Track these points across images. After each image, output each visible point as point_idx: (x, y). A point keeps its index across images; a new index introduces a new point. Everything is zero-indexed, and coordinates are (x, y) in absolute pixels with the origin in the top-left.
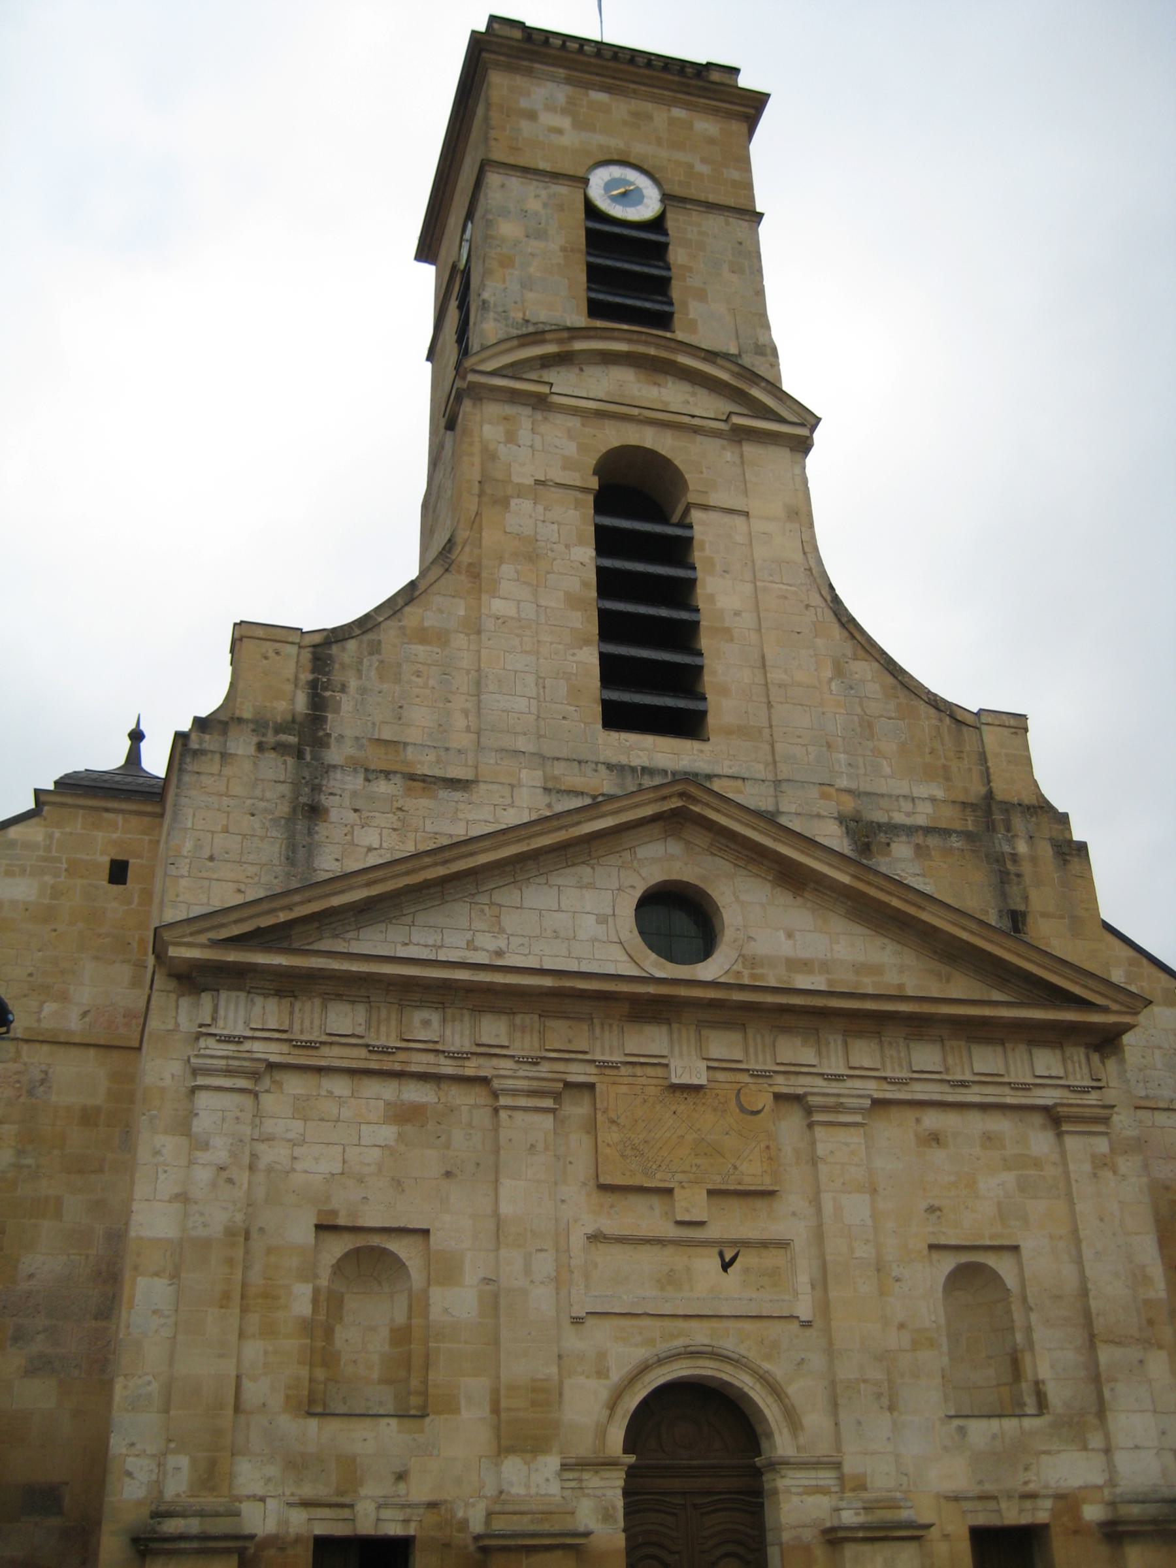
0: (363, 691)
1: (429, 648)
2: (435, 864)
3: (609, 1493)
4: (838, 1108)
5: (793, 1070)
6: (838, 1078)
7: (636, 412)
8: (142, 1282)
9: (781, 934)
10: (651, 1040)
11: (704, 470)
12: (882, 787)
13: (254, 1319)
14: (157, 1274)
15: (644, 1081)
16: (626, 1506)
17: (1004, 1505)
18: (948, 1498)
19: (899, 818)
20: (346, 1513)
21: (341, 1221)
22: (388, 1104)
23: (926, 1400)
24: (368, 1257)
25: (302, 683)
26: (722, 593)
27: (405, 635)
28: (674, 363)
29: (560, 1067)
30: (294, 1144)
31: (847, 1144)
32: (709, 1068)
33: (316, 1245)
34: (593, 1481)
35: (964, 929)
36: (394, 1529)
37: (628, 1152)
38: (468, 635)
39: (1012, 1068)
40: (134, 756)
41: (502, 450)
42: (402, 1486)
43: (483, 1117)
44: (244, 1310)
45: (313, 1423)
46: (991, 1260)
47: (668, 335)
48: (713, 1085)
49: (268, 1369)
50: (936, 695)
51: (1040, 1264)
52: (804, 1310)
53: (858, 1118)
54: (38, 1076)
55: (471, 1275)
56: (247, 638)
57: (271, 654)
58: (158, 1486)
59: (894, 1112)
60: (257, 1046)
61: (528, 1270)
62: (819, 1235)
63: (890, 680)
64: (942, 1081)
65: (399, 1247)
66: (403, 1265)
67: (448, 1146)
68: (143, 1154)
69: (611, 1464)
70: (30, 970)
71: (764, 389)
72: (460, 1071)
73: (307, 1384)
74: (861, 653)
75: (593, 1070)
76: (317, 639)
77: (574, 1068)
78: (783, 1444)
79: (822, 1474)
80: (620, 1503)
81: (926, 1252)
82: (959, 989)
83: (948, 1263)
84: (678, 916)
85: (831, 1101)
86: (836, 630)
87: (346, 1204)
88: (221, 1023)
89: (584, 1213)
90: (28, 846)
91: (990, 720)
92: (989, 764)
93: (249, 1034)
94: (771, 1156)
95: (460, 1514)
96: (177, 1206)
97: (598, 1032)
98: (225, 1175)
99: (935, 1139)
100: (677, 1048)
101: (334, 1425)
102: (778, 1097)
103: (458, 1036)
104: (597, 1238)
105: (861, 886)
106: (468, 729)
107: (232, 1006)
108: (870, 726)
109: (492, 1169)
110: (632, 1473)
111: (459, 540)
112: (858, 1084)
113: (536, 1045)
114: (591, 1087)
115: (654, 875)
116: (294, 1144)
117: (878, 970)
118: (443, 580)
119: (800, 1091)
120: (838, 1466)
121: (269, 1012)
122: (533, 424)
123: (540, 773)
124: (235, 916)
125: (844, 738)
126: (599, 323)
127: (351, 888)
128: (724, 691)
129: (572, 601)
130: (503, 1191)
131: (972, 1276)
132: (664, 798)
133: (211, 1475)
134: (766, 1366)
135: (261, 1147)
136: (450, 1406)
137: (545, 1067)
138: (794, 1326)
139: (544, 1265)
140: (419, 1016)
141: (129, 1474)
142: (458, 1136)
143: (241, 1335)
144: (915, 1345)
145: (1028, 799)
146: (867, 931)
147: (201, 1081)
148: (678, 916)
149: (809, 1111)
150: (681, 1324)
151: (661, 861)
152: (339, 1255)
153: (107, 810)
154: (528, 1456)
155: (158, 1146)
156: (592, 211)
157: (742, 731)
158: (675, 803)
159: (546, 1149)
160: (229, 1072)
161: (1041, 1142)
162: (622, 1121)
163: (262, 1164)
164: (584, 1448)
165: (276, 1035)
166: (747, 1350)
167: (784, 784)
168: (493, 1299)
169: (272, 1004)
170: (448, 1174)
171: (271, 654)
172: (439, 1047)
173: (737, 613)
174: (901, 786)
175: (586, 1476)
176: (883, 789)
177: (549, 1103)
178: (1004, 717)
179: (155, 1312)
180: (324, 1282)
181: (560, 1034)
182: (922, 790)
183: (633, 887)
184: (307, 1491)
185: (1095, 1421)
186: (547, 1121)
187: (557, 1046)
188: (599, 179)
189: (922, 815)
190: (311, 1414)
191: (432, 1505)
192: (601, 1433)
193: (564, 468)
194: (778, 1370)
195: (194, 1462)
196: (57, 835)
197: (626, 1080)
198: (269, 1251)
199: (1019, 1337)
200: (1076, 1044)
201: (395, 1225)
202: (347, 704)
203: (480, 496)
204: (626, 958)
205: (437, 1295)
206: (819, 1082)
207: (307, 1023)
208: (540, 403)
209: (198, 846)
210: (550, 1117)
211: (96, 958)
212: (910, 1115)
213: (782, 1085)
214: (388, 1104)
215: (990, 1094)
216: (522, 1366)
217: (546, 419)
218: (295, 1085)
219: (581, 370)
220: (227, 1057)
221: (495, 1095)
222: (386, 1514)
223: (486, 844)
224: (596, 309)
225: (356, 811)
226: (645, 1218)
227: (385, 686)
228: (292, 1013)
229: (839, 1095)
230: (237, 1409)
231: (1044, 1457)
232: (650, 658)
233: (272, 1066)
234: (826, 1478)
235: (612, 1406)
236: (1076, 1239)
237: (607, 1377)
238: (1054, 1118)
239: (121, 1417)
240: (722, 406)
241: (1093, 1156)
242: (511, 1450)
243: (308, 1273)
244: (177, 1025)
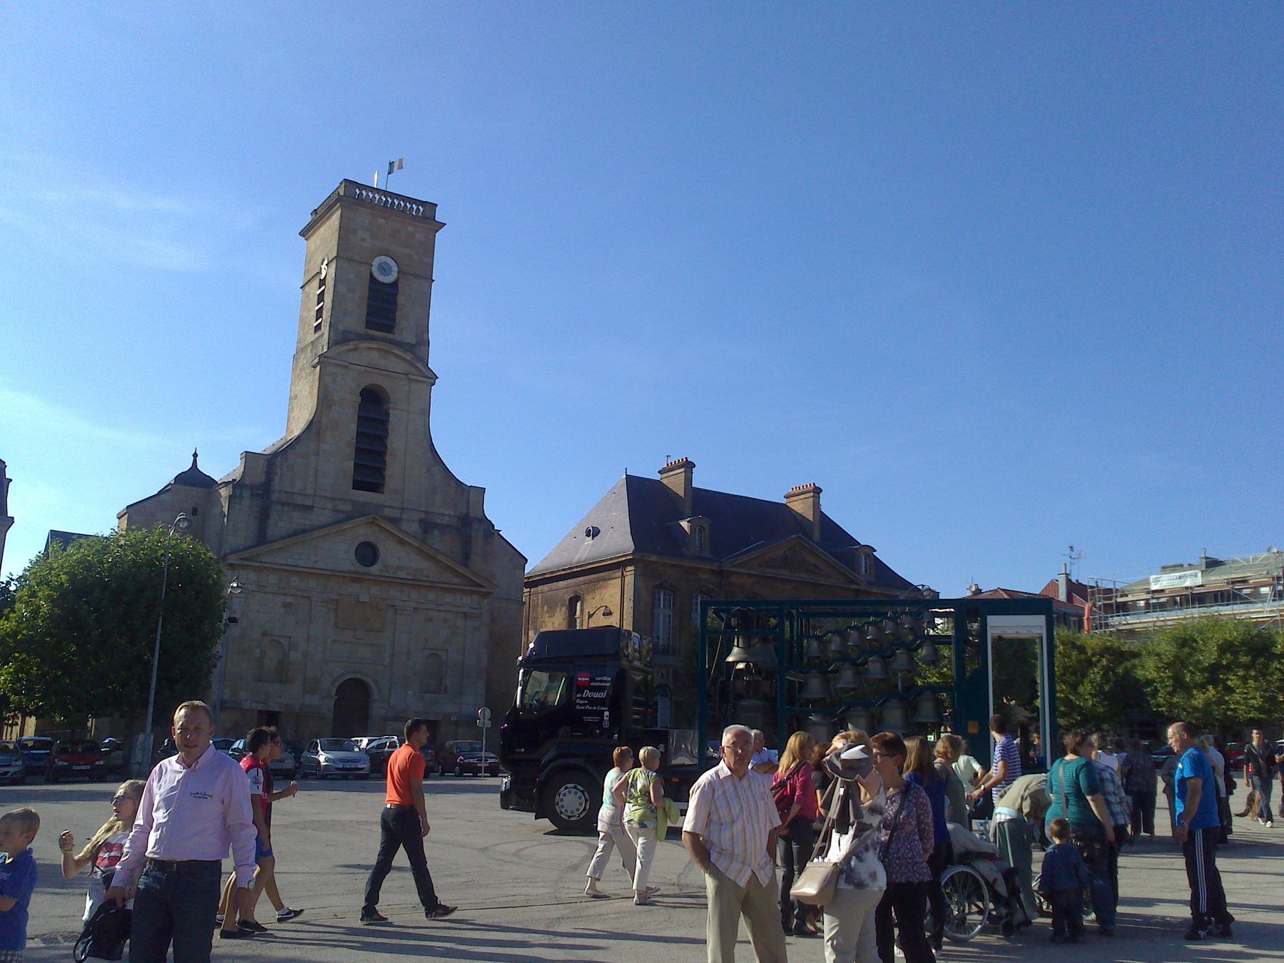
19: (438, 521)
26: (397, 442)
47: (390, 336)
56: (249, 457)
78: (376, 696)
84: (367, 553)
86: (430, 456)
99: (430, 619)
126: (369, 331)
145: (480, 516)
148: (367, 553)
151: (362, 532)
156: (371, 275)
188: (376, 262)
189: (446, 521)
198: (1179, 684)
202: (277, 479)
224: (369, 325)
232: (370, 465)
235: (333, 683)
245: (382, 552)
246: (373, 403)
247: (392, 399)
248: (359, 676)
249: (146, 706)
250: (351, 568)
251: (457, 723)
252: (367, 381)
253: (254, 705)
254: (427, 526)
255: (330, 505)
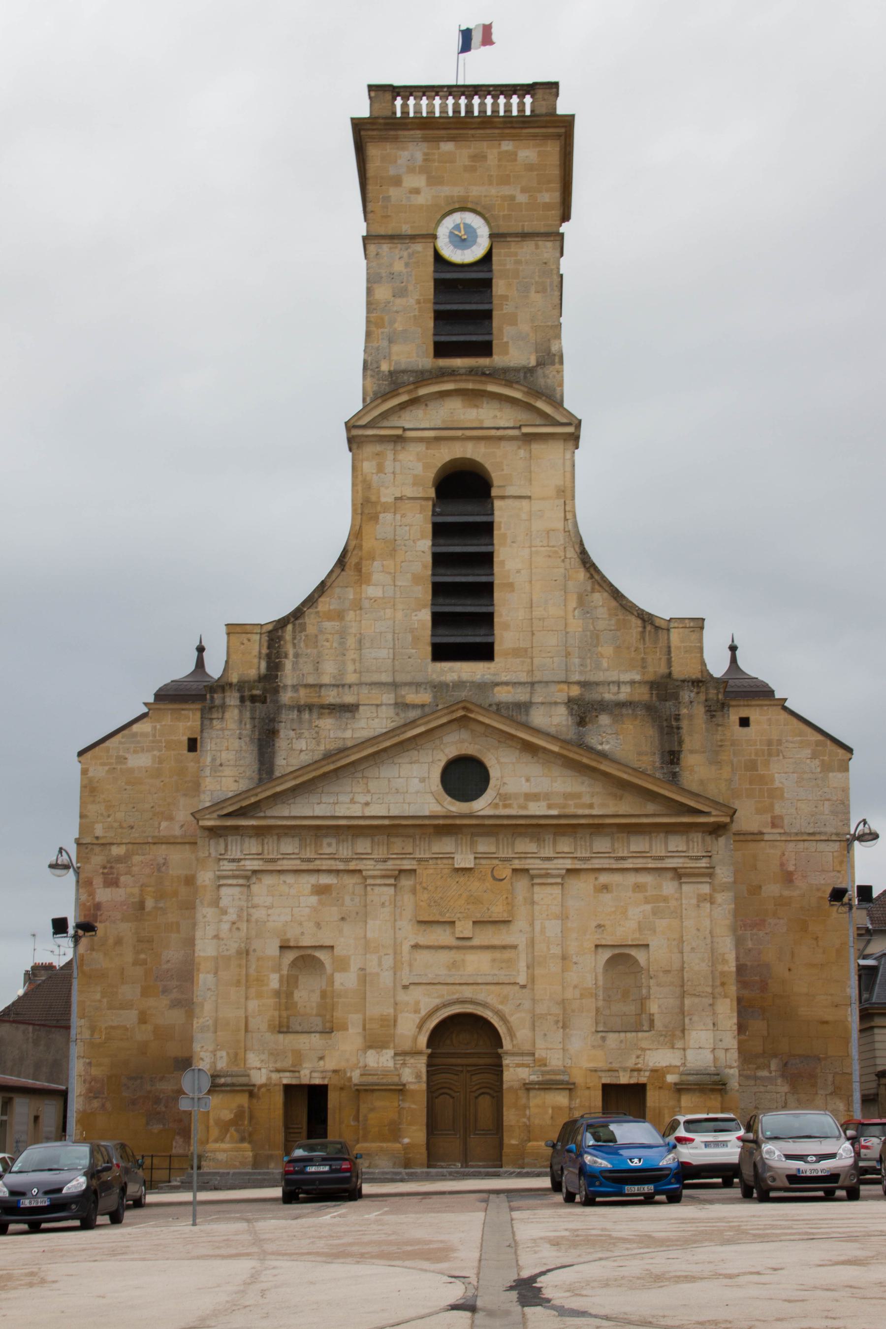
0: (297, 656)
1: (333, 623)
2: (328, 764)
3: (419, 1065)
4: (547, 875)
5: (523, 856)
6: (549, 859)
7: (459, 433)
8: (201, 976)
9: (523, 780)
10: (446, 845)
11: (505, 467)
12: (600, 676)
13: (252, 991)
14: (208, 972)
15: (442, 866)
16: (428, 1071)
17: (621, 1074)
18: (591, 1071)
19: (608, 696)
20: (297, 1074)
21: (292, 944)
22: (313, 885)
23: (584, 1023)
24: (305, 960)
25: (263, 656)
27: (319, 617)
28: (485, 391)
29: (398, 862)
30: (268, 908)
31: (551, 894)
32: (475, 858)
33: (280, 956)
34: (411, 1061)
35: (626, 773)
36: (317, 1081)
37: (432, 904)
38: (355, 611)
39: (654, 848)
40: (200, 663)
41: (375, 478)
42: (321, 1063)
43: (359, 889)
44: (247, 988)
45: (281, 1036)
46: (633, 952)
47: (482, 362)
48: (478, 867)
49: (260, 1010)
50: (643, 611)
51: (659, 953)
52: (522, 980)
53: (559, 880)
54: (162, 861)
55: (354, 967)
57: (245, 641)
58: (214, 1063)
59: (583, 876)
60: (248, 863)
61: (380, 964)
62: (532, 943)
63: (614, 603)
64: (609, 857)
65: (321, 955)
66: (323, 964)
67: (343, 905)
68: (199, 916)
69: (420, 1053)
70: (152, 805)
71: (545, 401)
72: (347, 868)
73: (278, 1019)
74: (597, 587)
75: (415, 862)
76: (270, 627)
77: (405, 862)
78: (507, 1044)
79: (526, 1058)
80: (424, 1070)
81: (593, 949)
82: (625, 807)
83: (607, 954)
84: (465, 776)
85: (543, 872)
87: (292, 935)
88: (229, 853)
89: (410, 934)
90: (144, 735)
91: (676, 625)
92: (672, 655)
93: (243, 857)
94: (510, 904)
95: (348, 1075)
96: (215, 941)
97: (418, 843)
98: (235, 926)
99: (605, 888)
100: (460, 849)
101: (290, 1037)
102: (515, 871)
103: (345, 851)
104: (416, 947)
105: (565, 752)
106: (355, 671)
107: (234, 844)
108: (598, 637)
109: (363, 914)
110: (430, 1057)
111: (350, 548)
112: (561, 861)
113: (385, 852)
114: (415, 871)
115: (452, 752)
116: (268, 908)
117: (578, 796)
118: (341, 577)
119: (527, 867)
120: (533, 1054)
121: (252, 846)
122: (394, 454)
123: (392, 696)
124: (230, 802)
125: (579, 648)
126: (444, 362)
127: (286, 781)
128: (506, 627)
129: (416, 579)
130: (368, 926)
131: (621, 960)
132: (453, 712)
133: (235, 1058)
134: (500, 1007)
135: (252, 911)
136: (344, 1028)
137: (390, 863)
138: (517, 988)
139: (388, 961)
140: (325, 841)
141: (202, 1059)
142: (347, 899)
143: (247, 998)
144: (582, 996)
146: (576, 774)
147: (222, 882)
148: (465, 776)
149: (532, 877)
150: (457, 987)
152: (292, 959)
153: (183, 709)
154: (379, 1050)
155: (205, 912)
157: (517, 652)
158: (461, 713)
159: (390, 904)
160: (235, 877)
161: (669, 887)
162: (429, 888)
163: (253, 919)
164: (407, 1046)
165: (256, 857)
166: (491, 1000)
167: (536, 685)
168: (364, 977)
169: (253, 841)
170: (343, 919)
171: (245, 641)
172: (336, 856)
173: (518, 571)
174: (613, 676)
175: (407, 1058)
176: (602, 679)
177: (392, 881)
178: (687, 621)
179: (209, 989)
180: (285, 972)
181: (398, 845)
182: (626, 677)
183: (440, 760)
184: (279, 1065)
185: (680, 1034)
186: (391, 890)
187: (396, 851)
188: (444, 231)
189: (624, 694)
190: (280, 1032)
191: (335, 1071)
192: (415, 1039)
193: (414, 484)
194: (506, 1009)
195: (228, 1054)
196: (158, 727)
197: (432, 867)
198: (258, 959)
199: (644, 991)
200: (697, 832)
201: (317, 944)
202: (288, 664)
203: (361, 514)
204: (434, 801)
205: (339, 978)
206: (538, 861)
207: (271, 848)
208: (398, 440)
209: (214, 760)
210: (393, 888)
211: (185, 795)
212: (591, 877)
213: (517, 864)
214: (313, 885)
215: (639, 863)
216: (377, 1008)
217: (403, 448)
218: (268, 880)
219: (426, 405)
220: (232, 870)
221: (365, 878)
222: (315, 1075)
223: (355, 750)
224: (441, 350)
225: (293, 730)
226: (442, 936)
227: (309, 651)
228: (263, 844)
229: (547, 869)
230: (246, 1030)
231: (648, 1052)
232: (463, 618)
233: (255, 872)
234: (528, 1060)
236: (681, 940)
237: (419, 1013)
238: (678, 874)
239: (198, 1036)
240: (522, 416)
241: (699, 895)
242: (370, 1047)
243: (278, 968)
244: (210, 854)
245: (494, 773)
246: (463, 490)
247: (496, 482)
248: (469, 1009)
249: (48, 1082)
250: (436, 809)
251: (680, 1089)
252: (446, 454)
253: (275, 1076)
254: (584, 711)
255: (388, 698)
